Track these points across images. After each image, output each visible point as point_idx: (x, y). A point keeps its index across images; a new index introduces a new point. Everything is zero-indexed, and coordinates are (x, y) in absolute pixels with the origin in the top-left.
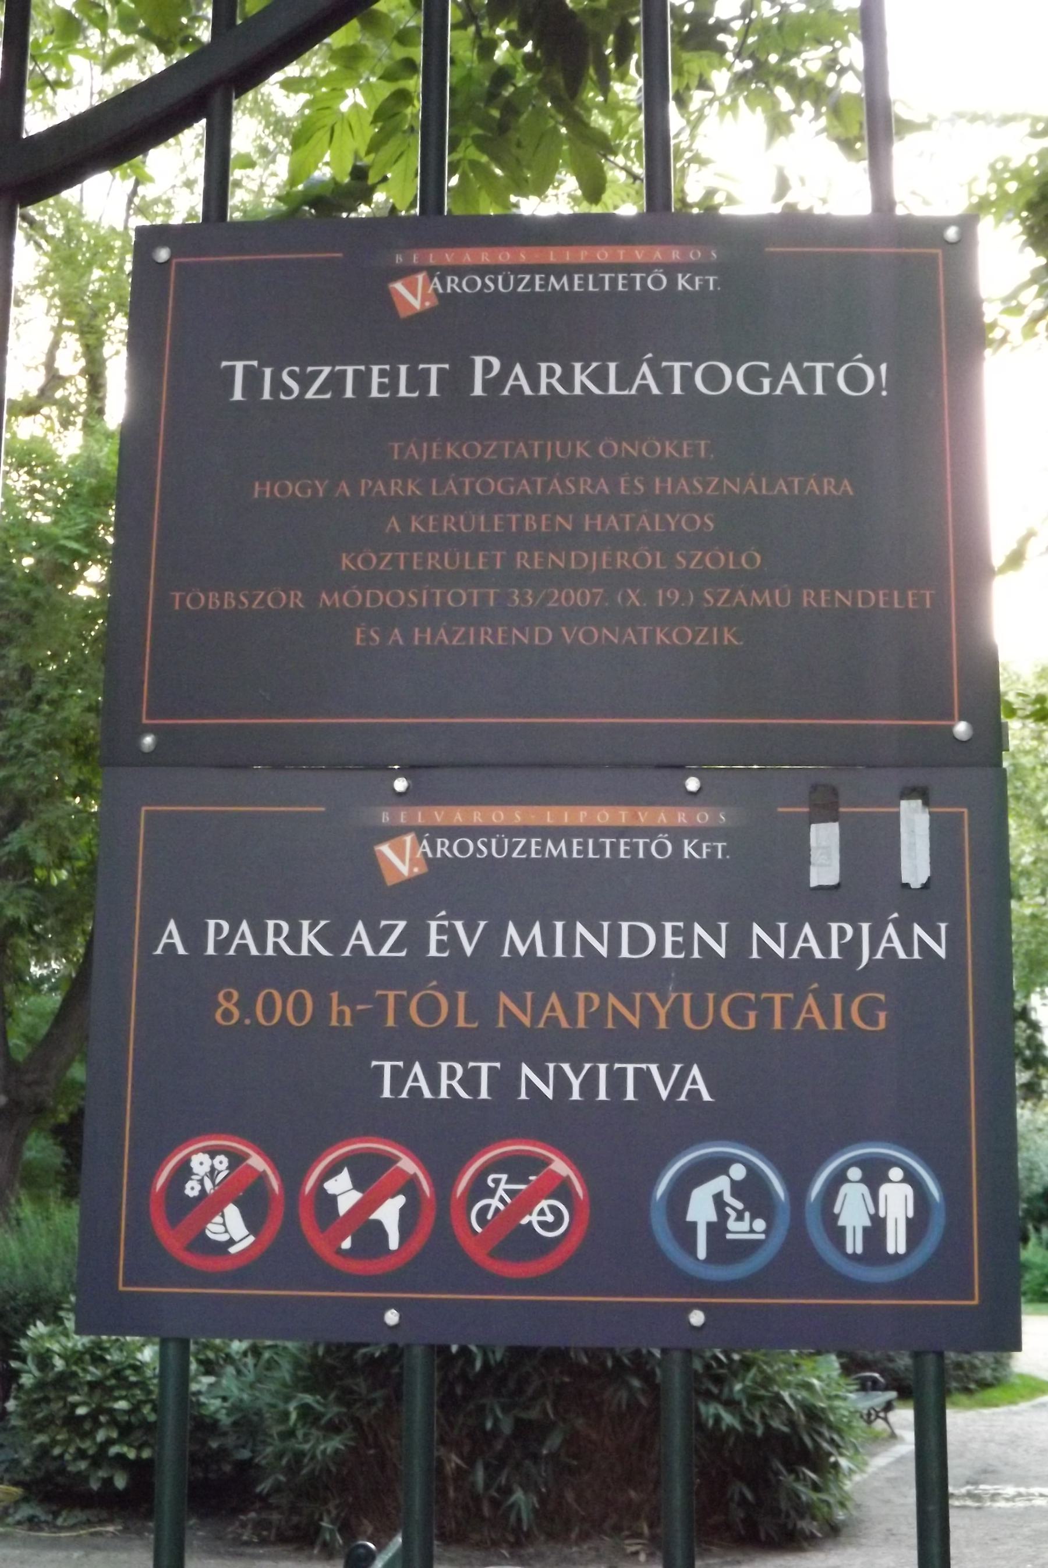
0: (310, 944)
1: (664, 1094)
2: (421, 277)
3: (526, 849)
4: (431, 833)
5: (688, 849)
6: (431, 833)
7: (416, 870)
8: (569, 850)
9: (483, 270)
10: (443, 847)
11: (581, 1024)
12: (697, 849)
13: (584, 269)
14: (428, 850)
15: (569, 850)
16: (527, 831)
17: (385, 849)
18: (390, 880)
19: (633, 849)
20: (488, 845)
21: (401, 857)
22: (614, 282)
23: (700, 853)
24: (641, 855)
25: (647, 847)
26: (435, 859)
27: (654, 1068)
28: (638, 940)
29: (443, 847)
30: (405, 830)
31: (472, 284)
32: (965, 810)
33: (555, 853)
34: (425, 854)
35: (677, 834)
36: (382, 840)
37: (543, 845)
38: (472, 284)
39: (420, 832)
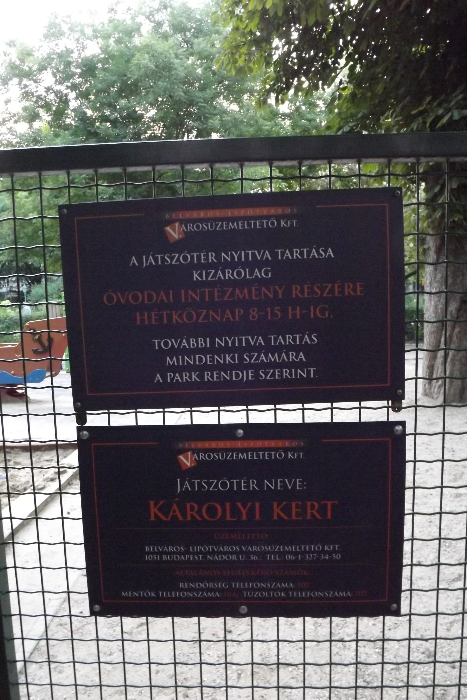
0: (155, 513)
1: (259, 258)
2: (177, 224)
3: (222, 226)
4: (196, 451)
5: (282, 223)
7: (181, 236)
8: (238, 226)
9: (202, 220)
10: (190, 227)
11: (237, 319)
12: (286, 223)
14: (184, 228)
15: (238, 226)
17: (168, 229)
19: (270, 455)
20: (218, 455)
21: (187, 459)
23: (294, 456)
24: (273, 458)
25: (275, 455)
26: (187, 232)
27: (256, 252)
29: (190, 227)
30: (176, 221)
31: (209, 456)
32: (388, 385)
33: (242, 458)
34: (195, 459)
36: (167, 226)
39: (181, 222)
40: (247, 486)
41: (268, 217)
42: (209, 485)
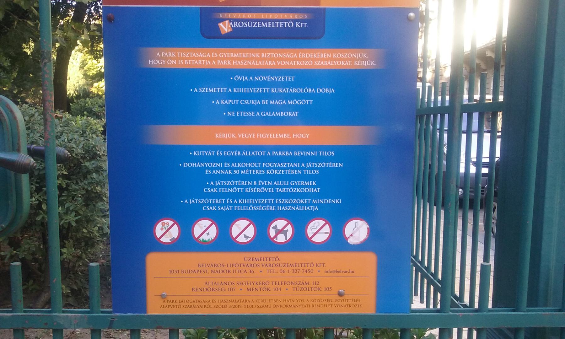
2: (227, 22)
3: (257, 25)
4: (232, 20)
6: (232, 20)
9: (244, 20)
10: (236, 24)
12: (300, 25)
13: (272, 20)
16: (257, 20)
17: (221, 25)
18: (223, 33)
20: (247, 24)
22: (279, 24)
25: (287, 24)
28: (326, 201)
30: (226, 20)
31: (241, 24)
35: (295, 21)
36: (220, 22)
37: (261, 23)
38: (241, 24)
39: (230, 20)
40: (237, 154)
41: (288, 20)
42: (201, 201)
